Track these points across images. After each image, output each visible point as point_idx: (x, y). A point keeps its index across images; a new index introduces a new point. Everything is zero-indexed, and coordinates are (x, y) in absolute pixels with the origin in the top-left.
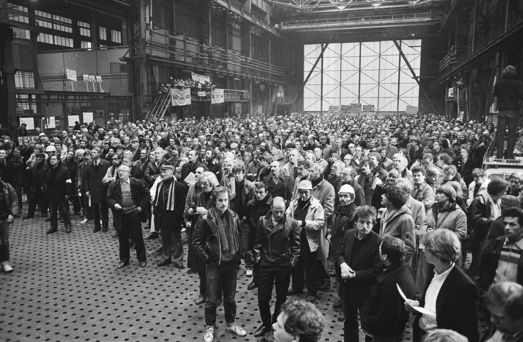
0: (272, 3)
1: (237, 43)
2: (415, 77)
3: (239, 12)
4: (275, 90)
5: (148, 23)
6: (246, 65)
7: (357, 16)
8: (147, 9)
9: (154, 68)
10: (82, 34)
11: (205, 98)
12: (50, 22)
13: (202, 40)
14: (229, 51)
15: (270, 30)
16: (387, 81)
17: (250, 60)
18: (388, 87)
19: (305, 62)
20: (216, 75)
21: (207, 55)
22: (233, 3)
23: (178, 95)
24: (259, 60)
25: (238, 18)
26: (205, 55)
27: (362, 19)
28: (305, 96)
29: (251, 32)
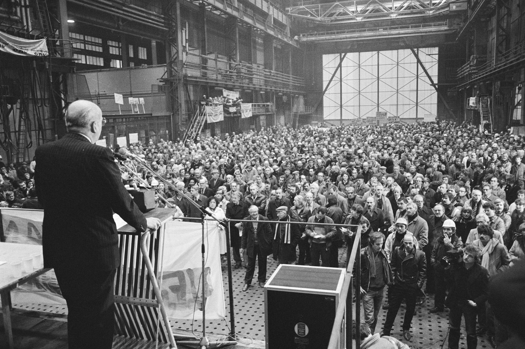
0: (291, 16)
1: (260, 57)
2: (433, 84)
3: (263, 28)
4: (296, 100)
5: (185, 45)
6: (269, 78)
7: (376, 26)
8: (184, 31)
9: (189, 87)
10: (111, 53)
11: (235, 113)
12: (82, 43)
13: (230, 57)
14: (254, 66)
15: (290, 42)
16: (406, 88)
17: (273, 73)
18: (406, 94)
19: (324, 71)
20: (244, 90)
21: (235, 71)
22: (258, 20)
23: (213, 112)
24: (281, 72)
25: (261, 33)
26: (232, 71)
27: (380, 30)
28: (324, 105)
29: (274, 45)
